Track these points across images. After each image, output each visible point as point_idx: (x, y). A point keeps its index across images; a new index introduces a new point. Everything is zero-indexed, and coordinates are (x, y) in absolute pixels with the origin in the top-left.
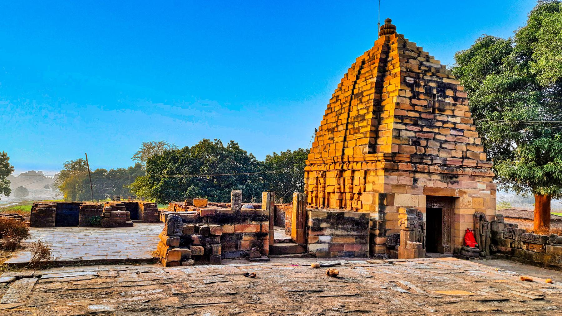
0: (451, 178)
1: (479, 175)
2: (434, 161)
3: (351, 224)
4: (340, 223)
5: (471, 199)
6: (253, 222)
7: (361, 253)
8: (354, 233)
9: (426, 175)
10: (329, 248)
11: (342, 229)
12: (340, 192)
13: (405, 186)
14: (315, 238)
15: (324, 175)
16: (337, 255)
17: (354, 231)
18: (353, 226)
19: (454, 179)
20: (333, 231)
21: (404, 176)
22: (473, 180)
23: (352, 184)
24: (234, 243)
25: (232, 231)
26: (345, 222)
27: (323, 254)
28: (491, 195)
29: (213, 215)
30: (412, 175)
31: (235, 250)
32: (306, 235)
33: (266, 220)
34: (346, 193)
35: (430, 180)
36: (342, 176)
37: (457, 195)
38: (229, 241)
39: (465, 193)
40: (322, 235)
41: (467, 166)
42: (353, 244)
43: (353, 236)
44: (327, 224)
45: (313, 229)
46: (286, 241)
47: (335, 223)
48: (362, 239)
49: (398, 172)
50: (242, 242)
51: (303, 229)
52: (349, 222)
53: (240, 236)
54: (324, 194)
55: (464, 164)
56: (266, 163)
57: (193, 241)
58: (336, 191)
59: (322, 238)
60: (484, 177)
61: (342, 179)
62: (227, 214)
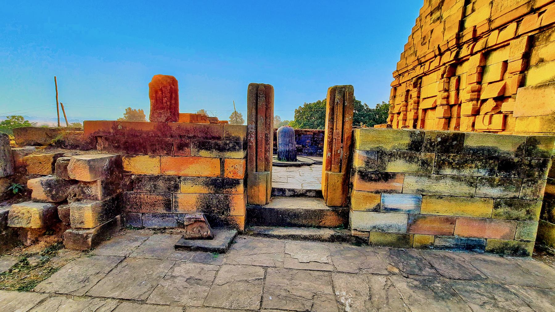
3: (484, 167)
4: (451, 163)
6: (203, 153)
7: (506, 244)
8: (496, 192)
10: (409, 225)
11: (453, 178)
12: (448, 104)
14: (367, 199)
15: (418, 83)
16: (432, 244)
17: (492, 186)
18: (491, 172)
20: (425, 184)
23: (479, 82)
24: (161, 198)
25: (156, 172)
26: (466, 161)
27: (389, 239)
29: (110, 133)
31: (165, 212)
32: (347, 186)
33: (233, 149)
34: (460, 105)
36: (454, 75)
38: (150, 191)
40: (391, 192)
42: (484, 220)
43: (486, 198)
44: (408, 164)
45: (364, 176)
46: (308, 194)
47: (433, 164)
48: (517, 209)
50: (178, 196)
51: (343, 173)
52: (480, 160)
53: (173, 183)
54: (417, 113)
56: (376, 109)
57: (30, 192)
58: (438, 103)
59: (390, 201)
61: (454, 80)
62: (141, 132)
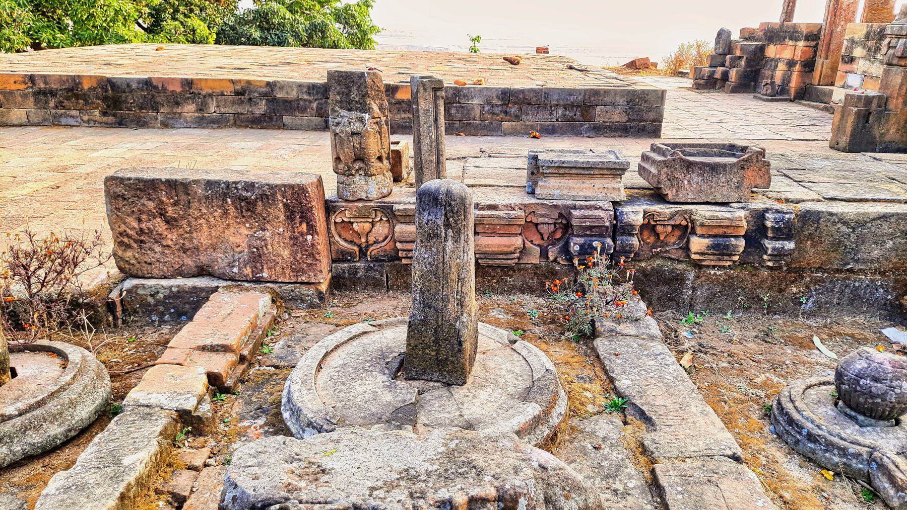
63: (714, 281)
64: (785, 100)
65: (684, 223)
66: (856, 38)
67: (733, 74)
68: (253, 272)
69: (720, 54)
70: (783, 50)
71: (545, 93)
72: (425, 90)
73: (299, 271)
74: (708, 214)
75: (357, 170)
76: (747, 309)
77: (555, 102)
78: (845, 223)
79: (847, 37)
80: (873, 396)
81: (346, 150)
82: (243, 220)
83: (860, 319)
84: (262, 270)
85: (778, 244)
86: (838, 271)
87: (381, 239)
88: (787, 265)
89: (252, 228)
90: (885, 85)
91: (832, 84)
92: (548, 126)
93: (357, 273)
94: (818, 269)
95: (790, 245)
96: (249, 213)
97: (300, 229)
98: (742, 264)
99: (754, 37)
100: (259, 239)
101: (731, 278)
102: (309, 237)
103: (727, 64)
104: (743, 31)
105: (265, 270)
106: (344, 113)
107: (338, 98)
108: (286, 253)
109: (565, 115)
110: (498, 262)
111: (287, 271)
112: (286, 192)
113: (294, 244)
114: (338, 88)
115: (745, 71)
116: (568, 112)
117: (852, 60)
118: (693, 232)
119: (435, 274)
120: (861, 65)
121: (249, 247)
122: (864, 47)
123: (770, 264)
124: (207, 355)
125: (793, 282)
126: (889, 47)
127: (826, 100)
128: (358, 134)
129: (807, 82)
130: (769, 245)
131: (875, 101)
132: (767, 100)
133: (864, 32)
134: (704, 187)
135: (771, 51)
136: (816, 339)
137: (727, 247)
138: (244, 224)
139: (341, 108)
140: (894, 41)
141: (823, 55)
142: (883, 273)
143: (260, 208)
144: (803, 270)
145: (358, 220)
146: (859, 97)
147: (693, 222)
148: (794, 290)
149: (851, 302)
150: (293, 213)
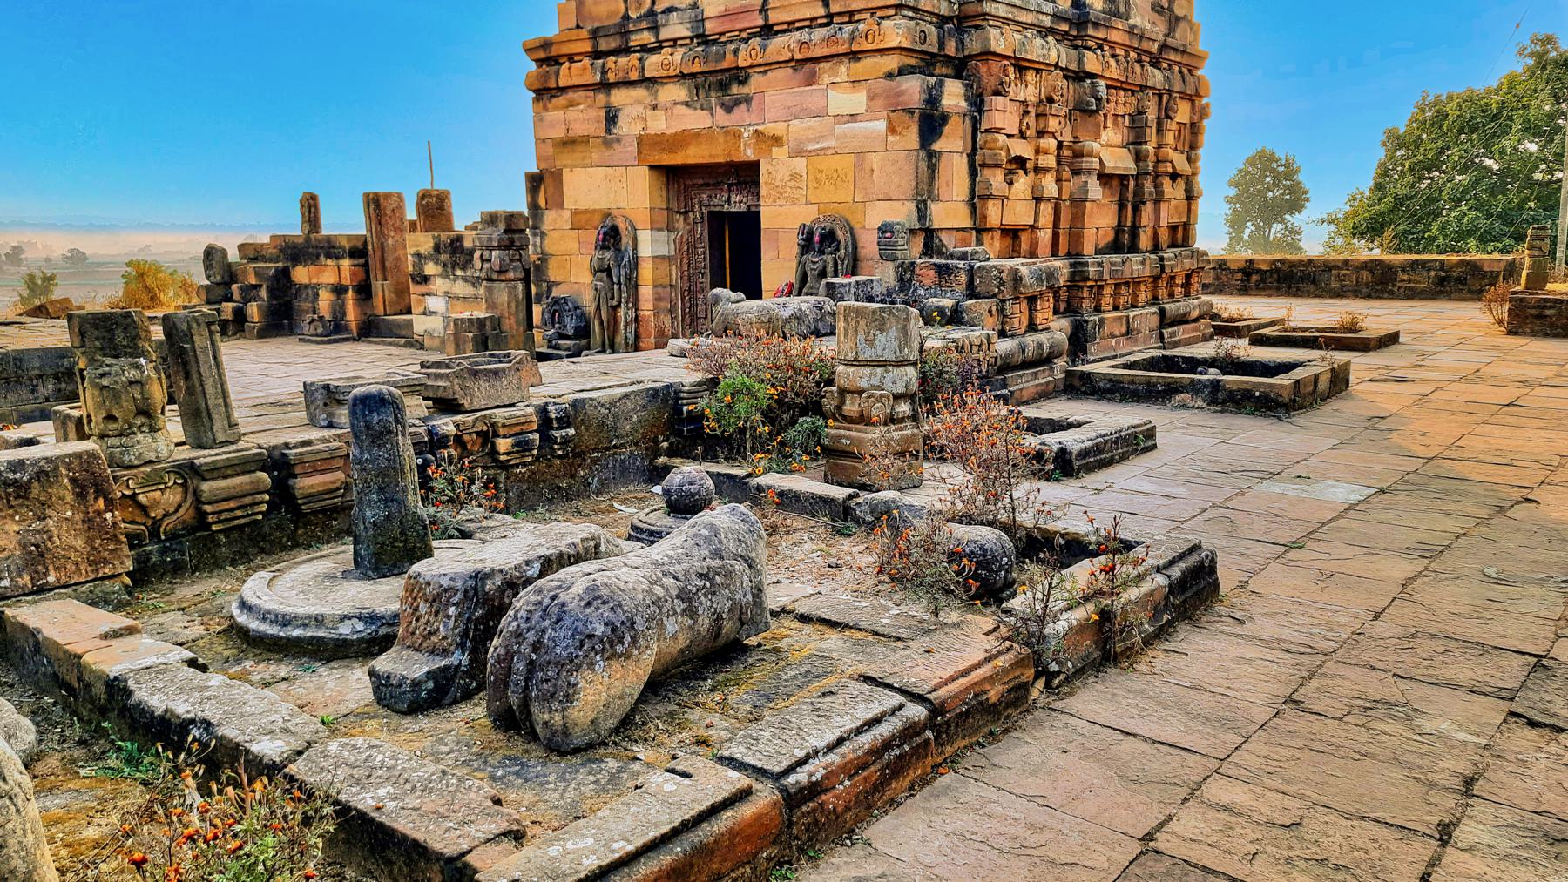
0: (723, 87)
1: (826, 52)
2: (665, 34)
5: (800, 164)
9: (640, 92)
13: (585, 140)
19: (735, 89)
21: (581, 107)
22: (811, 80)
28: (891, 138)
30: (601, 98)
35: (655, 107)
37: (749, 154)
39: (777, 141)
41: (793, 22)
49: (564, 96)
55: (774, 17)
60: (854, 56)
63: (520, 479)
64: (347, 339)
65: (485, 428)
66: (422, 251)
67: (253, 310)
68: (32, 579)
69: (218, 284)
70: (320, 272)
71: (15, 359)
72: (199, 325)
73: (100, 562)
74: (506, 414)
75: (139, 427)
76: (550, 501)
77: (37, 372)
78: (603, 405)
79: (410, 251)
80: (693, 495)
81: (125, 404)
82: (11, 511)
83: (631, 488)
84: (46, 575)
85: (563, 432)
86: (607, 449)
87: (172, 510)
88: (572, 451)
89: (24, 521)
90: (491, 305)
91: (409, 312)
92: (32, 411)
93: (149, 559)
94: (594, 450)
95: (572, 432)
96: (20, 501)
97: (96, 507)
98: (537, 459)
99: (263, 257)
100: (38, 532)
101: (534, 473)
102: (108, 515)
103: (236, 296)
104: (241, 247)
105: (52, 573)
106: (109, 361)
107: (97, 344)
108: (79, 543)
109: (60, 390)
110: (324, 503)
111: (83, 567)
112: (71, 462)
113: (89, 528)
114: (96, 332)
115: (270, 306)
116: (63, 385)
117: (425, 279)
118: (496, 435)
119: (394, 468)
120: (440, 284)
121: (24, 546)
122: (437, 262)
123: (560, 452)
124: (115, 643)
125: (579, 466)
126: (483, 261)
127: (403, 333)
128: (137, 382)
129: (369, 312)
130: (558, 434)
131: (488, 323)
132: (318, 343)
133: (432, 244)
134: (492, 391)
135: (301, 274)
136: (615, 505)
137: (527, 442)
138: (12, 517)
139: (104, 355)
140: (486, 253)
141: (379, 276)
142: (636, 444)
143: (36, 492)
144: (583, 452)
145: (146, 489)
146: (470, 320)
147: (493, 425)
148: (582, 473)
149: (622, 473)
150: (83, 488)
